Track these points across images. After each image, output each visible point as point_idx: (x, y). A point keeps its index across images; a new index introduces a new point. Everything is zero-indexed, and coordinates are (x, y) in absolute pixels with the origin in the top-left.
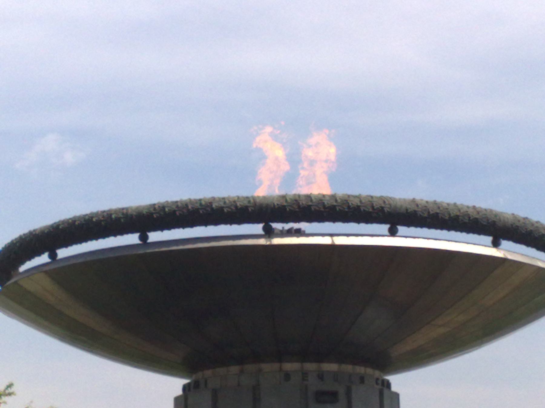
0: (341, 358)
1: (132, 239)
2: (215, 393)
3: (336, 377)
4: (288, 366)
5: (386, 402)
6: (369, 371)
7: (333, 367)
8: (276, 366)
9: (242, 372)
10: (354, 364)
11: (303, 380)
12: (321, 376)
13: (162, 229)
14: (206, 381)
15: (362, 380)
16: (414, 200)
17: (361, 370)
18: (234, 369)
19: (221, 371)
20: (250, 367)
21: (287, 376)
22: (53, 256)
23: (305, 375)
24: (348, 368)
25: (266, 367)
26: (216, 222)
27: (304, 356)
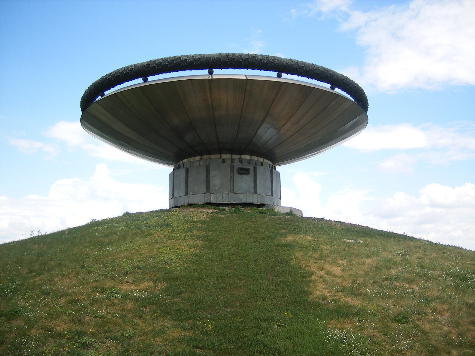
0: (252, 153)
1: (139, 81)
2: (187, 170)
3: (249, 162)
4: (224, 156)
5: (274, 176)
6: (266, 161)
7: (248, 157)
8: (218, 156)
9: (201, 159)
10: (258, 156)
11: (232, 163)
12: (241, 161)
13: (120, 84)
14: (183, 164)
15: (262, 164)
16: (291, 59)
17: (261, 159)
18: (197, 158)
19: (191, 159)
20: (205, 157)
21: (224, 161)
22: (145, 80)
23: (233, 160)
24: (255, 158)
25: (213, 156)
26: (183, 69)
27: (232, 151)
